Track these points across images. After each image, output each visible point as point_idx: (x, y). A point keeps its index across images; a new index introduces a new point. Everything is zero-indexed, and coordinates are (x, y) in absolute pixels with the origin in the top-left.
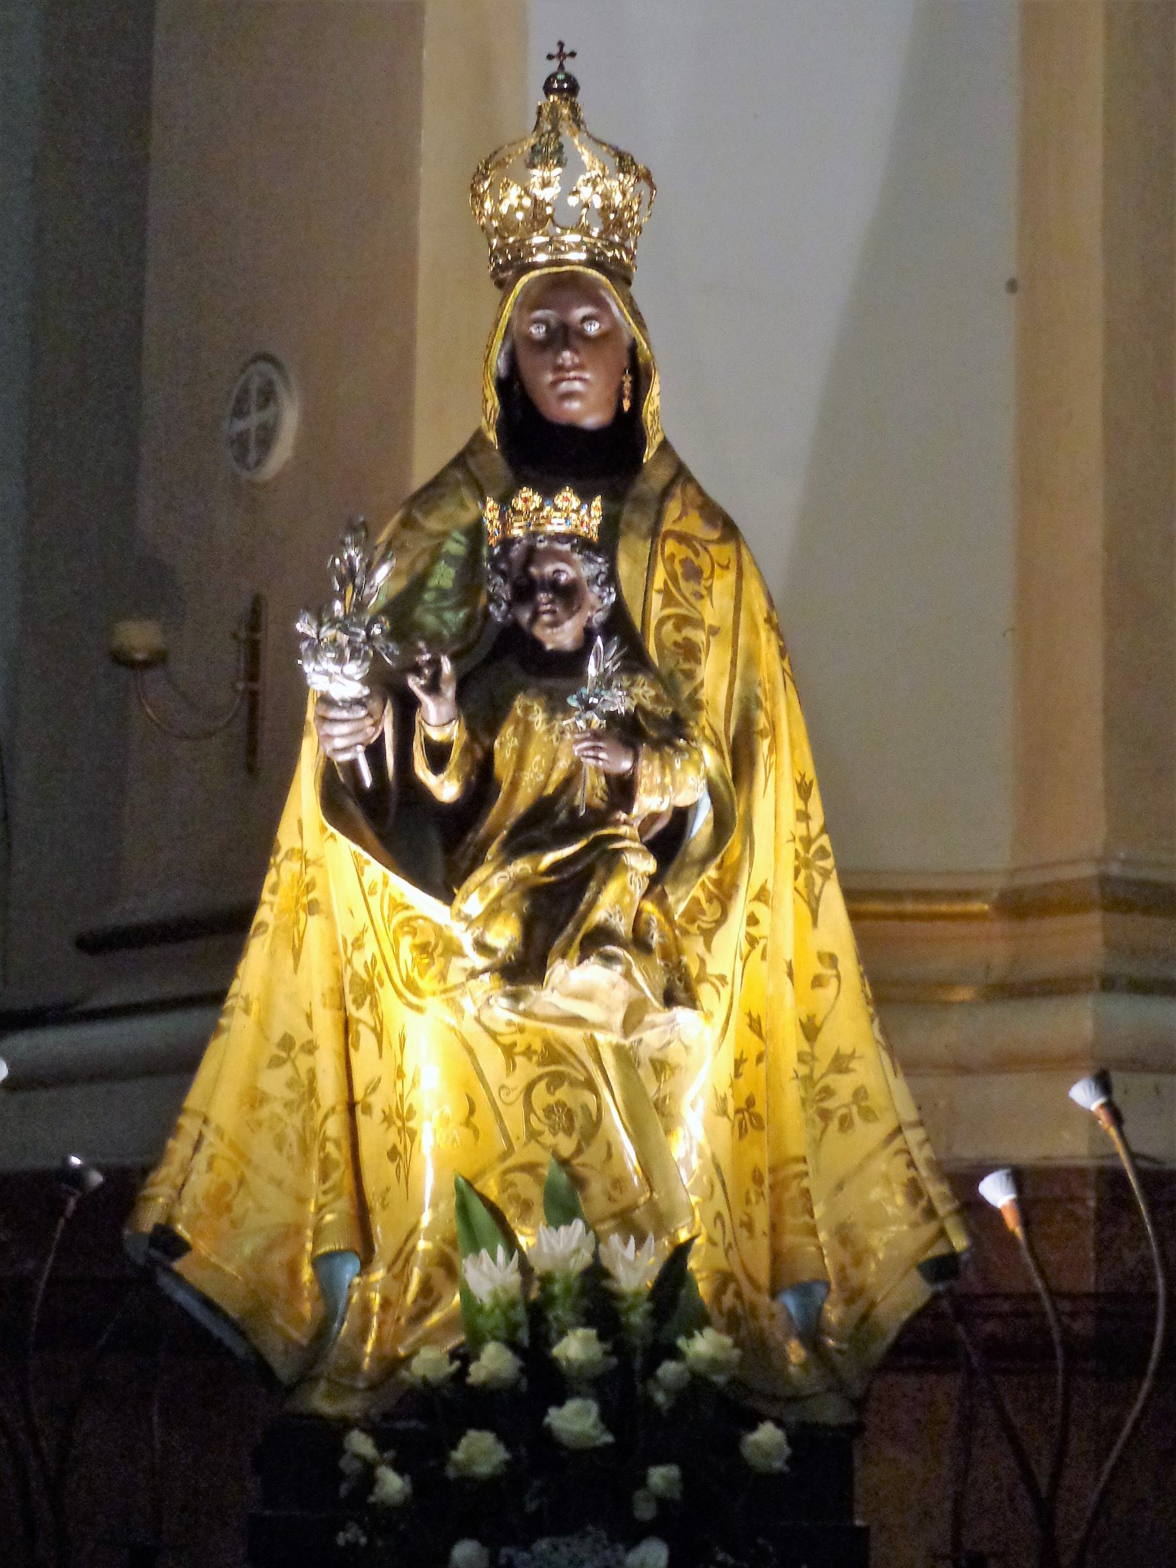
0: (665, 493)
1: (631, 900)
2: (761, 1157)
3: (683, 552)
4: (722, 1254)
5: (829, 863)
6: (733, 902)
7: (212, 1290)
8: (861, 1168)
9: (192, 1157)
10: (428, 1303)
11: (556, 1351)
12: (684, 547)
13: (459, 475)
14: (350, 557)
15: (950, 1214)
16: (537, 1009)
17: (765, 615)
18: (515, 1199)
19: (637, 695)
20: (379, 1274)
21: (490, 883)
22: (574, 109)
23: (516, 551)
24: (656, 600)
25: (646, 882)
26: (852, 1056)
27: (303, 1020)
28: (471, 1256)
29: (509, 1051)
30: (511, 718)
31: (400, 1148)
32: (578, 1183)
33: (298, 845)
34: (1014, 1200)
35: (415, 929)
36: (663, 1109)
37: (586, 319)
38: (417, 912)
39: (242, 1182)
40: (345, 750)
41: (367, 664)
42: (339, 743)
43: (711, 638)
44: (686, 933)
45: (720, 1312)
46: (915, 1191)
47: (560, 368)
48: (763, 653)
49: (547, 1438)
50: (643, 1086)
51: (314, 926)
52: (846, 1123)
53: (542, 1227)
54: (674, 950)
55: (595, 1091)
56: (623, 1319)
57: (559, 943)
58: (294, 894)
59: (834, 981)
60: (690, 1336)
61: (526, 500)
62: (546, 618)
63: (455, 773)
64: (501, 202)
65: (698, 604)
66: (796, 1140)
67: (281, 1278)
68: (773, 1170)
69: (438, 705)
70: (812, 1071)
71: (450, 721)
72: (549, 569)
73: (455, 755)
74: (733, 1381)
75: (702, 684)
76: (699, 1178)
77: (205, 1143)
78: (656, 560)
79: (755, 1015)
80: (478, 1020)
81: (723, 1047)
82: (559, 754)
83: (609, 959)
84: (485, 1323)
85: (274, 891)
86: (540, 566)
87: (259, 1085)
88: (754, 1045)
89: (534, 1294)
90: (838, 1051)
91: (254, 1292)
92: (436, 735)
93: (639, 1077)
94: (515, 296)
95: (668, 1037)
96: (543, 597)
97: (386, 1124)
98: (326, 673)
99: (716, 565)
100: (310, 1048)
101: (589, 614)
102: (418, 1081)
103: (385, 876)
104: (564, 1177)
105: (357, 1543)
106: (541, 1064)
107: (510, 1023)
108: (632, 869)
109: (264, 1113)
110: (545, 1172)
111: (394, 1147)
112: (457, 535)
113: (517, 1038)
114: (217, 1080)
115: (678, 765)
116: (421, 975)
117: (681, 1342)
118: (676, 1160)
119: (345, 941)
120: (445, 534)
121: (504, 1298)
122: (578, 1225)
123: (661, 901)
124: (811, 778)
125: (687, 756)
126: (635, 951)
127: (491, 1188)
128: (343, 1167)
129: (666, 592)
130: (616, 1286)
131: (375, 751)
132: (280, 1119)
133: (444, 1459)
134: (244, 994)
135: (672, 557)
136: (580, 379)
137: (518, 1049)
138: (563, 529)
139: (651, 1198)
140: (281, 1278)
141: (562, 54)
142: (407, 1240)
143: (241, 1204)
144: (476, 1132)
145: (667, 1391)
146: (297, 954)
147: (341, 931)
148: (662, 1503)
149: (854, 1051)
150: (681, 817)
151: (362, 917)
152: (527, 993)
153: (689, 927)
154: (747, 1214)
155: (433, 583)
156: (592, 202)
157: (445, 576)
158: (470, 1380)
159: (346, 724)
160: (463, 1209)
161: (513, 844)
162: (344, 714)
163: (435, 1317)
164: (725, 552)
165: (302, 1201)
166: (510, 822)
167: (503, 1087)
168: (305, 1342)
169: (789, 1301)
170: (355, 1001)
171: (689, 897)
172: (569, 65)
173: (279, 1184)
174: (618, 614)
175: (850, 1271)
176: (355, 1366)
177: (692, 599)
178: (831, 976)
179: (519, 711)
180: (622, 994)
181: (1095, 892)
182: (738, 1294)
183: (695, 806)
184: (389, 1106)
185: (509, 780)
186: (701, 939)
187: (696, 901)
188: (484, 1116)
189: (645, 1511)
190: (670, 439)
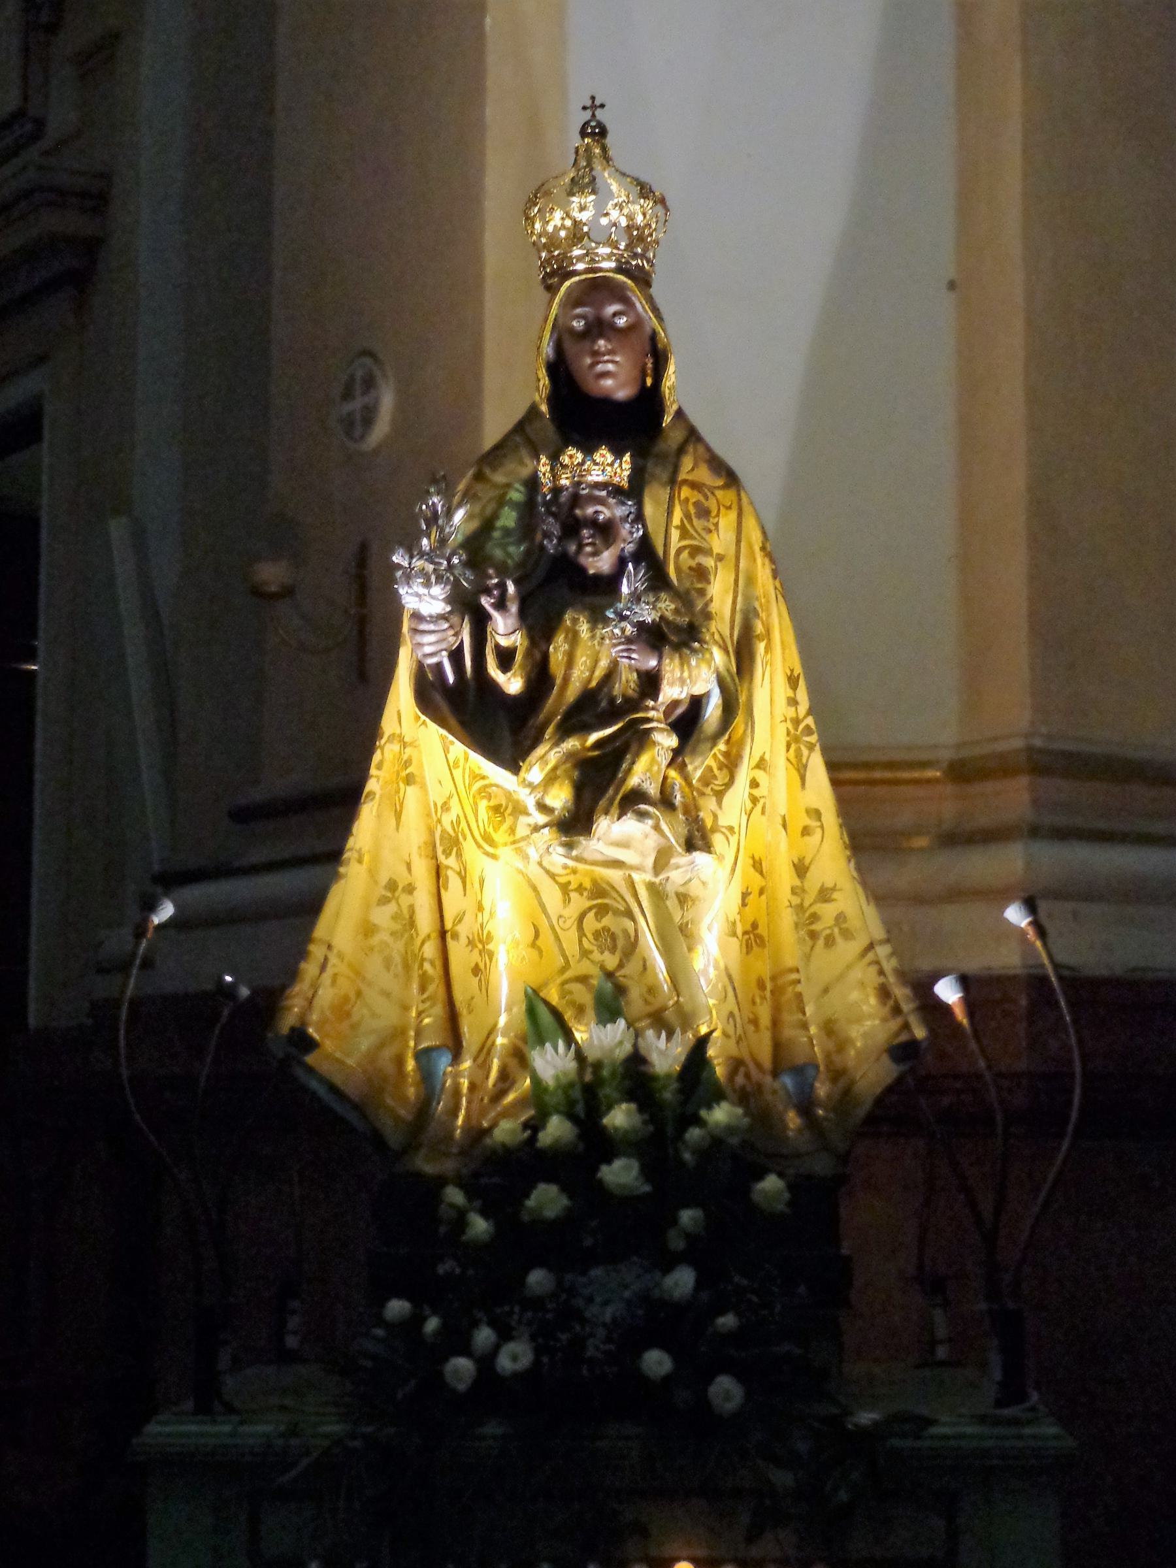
0: (681, 450)
2: (763, 968)
3: (695, 496)
5: (813, 739)
6: (738, 769)
8: (841, 977)
11: (605, 1121)
12: (696, 493)
13: (518, 439)
14: (433, 503)
16: (586, 855)
17: (761, 545)
18: (572, 1003)
19: (660, 608)
20: (467, 1064)
22: (604, 149)
23: (564, 497)
26: (834, 889)
27: (404, 868)
29: (565, 888)
31: (482, 966)
32: (621, 990)
33: (398, 731)
36: (686, 931)
37: (615, 314)
39: (359, 994)
40: (432, 655)
41: (448, 587)
42: (428, 650)
44: (703, 794)
46: (884, 993)
48: (759, 574)
52: (830, 942)
53: (593, 1025)
55: (633, 919)
57: (603, 803)
58: (395, 770)
59: (819, 831)
60: (709, 1107)
61: (571, 457)
62: (588, 549)
63: (519, 672)
66: (791, 958)
67: (390, 1068)
68: (773, 978)
69: (505, 618)
70: (802, 900)
71: (513, 632)
72: (590, 510)
73: (519, 657)
75: (711, 600)
77: (329, 965)
79: (757, 858)
80: (540, 864)
83: (642, 815)
84: (551, 1100)
85: (379, 767)
86: (582, 508)
88: (757, 881)
89: (588, 1077)
92: (504, 642)
96: (585, 532)
97: (470, 948)
98: (417, 595)
100: (410, 889)
101: (622, 546)
103: (465, 753)
104: (609, 985)
106: (590, 898)
107: (565, 867)
109: (375, 940)
110: (595, 982)
111: (477, 965)
112: (517, 486)
114: (337, 915)
115: (693, 663)
116: (495, 830)
117: (703, 1113)
119: (435, 805)
120: (508, 486)
121: (564, 1081)
122: (621, 1023)
123: (682, 768)
125: (700, 655)
127: (554, 997)
128: (437, 981)
131: (456, 656)
134: (357, 847)
135: (687, 500)
136: (612, 362)
138: (600, 479)
139: (677, 1002)
141: (594, 106)
142: (488, 1037)
143: (359, 1012)
146: (398, 815)
147: (432, 798)
148: (687, 1236)
150: (697, 703)
152: (579, 842)
155: (500, 523)
159: (433, 635)
160: (531, 1012)
162: (432, 627)
163: (511, 1097)
165: (406, 1008)
167: (560, 916)
169: (788, 1081)
170: (444, 852)
172: (599, 113)
173: (387, 994)
176: (450, 1136)
177: (703, 534)
180: (652, 842)
182: (747, 1076)
183: (707, 695)
185: (561, 676)
186: (714, 799)
188: (547, 939)
189: (677, 1243)
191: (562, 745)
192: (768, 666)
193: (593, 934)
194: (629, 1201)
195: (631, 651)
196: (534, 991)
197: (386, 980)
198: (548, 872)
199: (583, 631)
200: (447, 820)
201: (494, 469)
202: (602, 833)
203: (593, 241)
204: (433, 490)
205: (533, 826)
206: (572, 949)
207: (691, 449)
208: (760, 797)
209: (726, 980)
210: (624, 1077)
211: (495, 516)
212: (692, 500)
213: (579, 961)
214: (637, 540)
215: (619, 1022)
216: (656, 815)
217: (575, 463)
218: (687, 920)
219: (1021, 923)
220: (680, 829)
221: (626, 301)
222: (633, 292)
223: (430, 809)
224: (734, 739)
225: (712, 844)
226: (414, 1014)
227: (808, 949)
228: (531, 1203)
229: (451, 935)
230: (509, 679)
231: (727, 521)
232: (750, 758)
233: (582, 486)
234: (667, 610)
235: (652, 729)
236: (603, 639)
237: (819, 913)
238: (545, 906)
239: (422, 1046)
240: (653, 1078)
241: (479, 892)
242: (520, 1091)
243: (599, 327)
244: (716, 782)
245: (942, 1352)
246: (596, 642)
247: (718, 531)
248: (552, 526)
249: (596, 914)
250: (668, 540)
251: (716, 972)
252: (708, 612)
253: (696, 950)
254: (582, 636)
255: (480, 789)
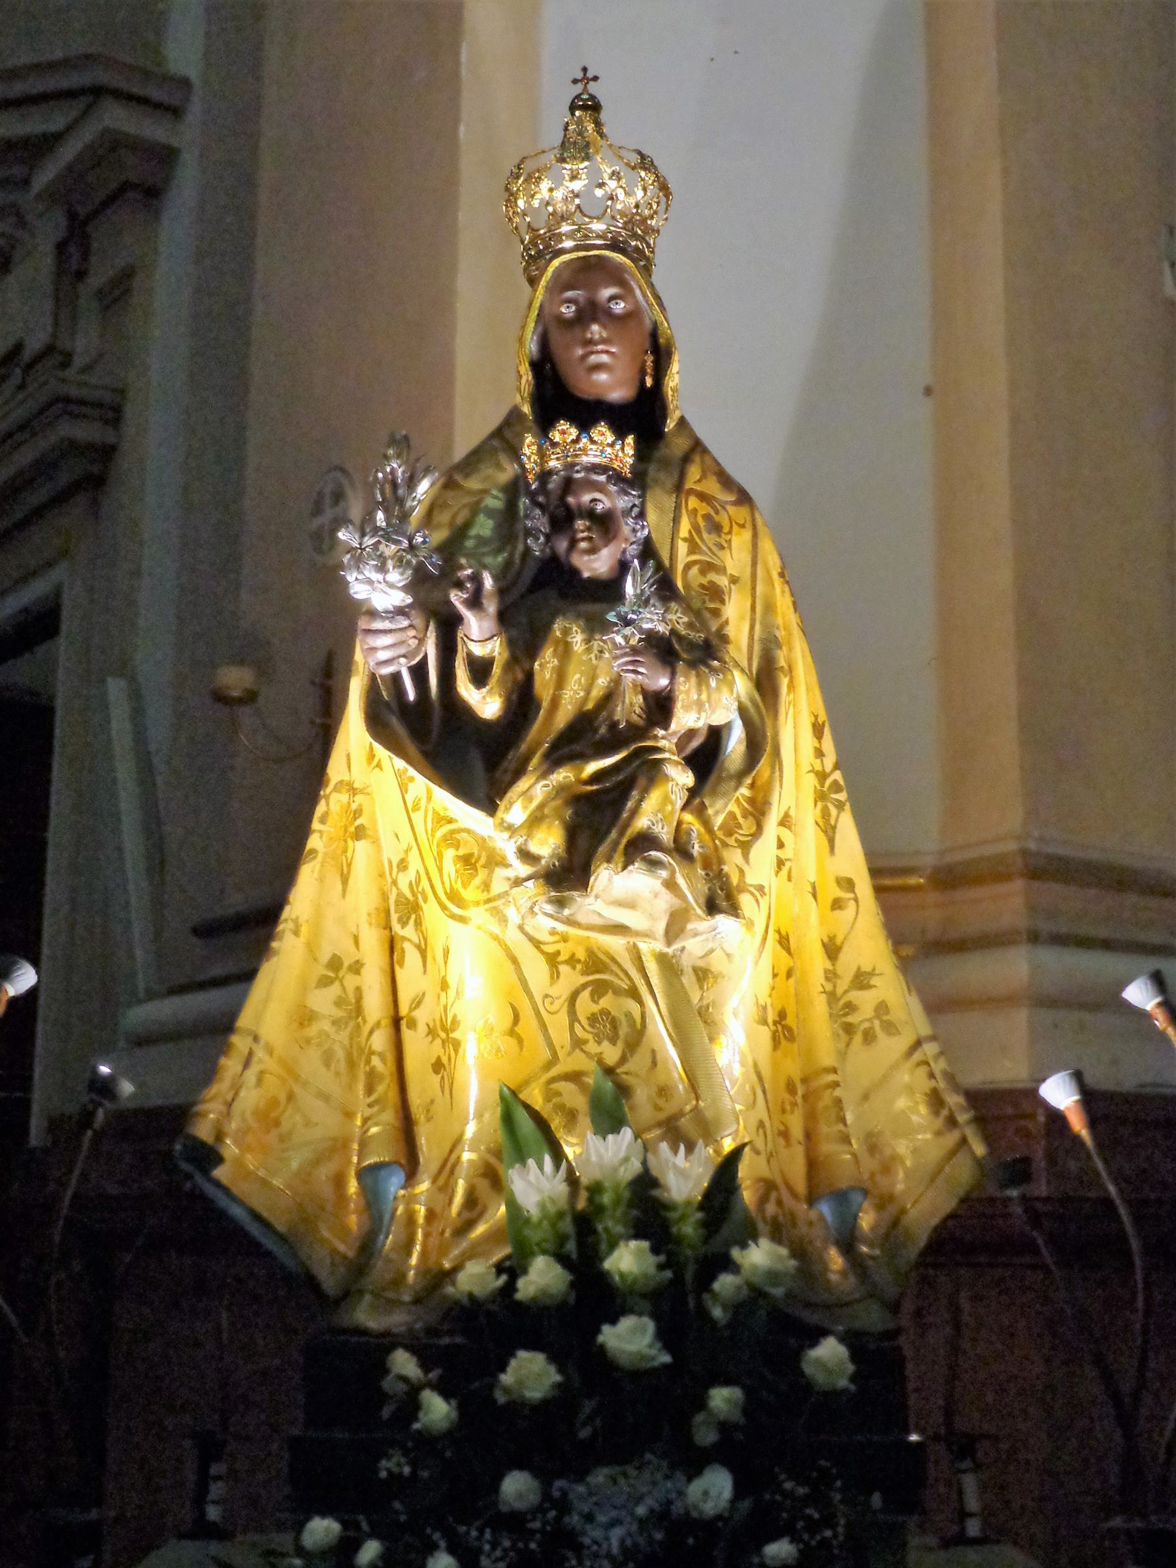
0: (686, 459)
1: (672, 809)
2: (793, 1068)
3: (704, 509)
4: (764, 1162)
5: (842, 796)
6: (767, 818)
7: (258, 1203)
8: (885, 1079)
9: (242, 1073)
10: (474, 1214)
11: (608, 1264)
12: (704, 504)
13: (495, 443)
14: (393, 469)
15: (969, 1122)
16: (581, 918)
17: (780, 570)
18: (560, 1108)
19: (671, 620)
20: (423, 1186)
21: (532, 791)
22: (598, 124)
23: (554, 484)
24: (682, 548)
25: (685, 795)
26: (872, 974)
27: (351, 942)
28: (517, 1166)
29: (552, 960)
30: (550, 638)
31: (445, 1060)
32: (623, 1091)
33: (347, 778)
34: (1077, 1102)
35: (458, 841)
36: (707, 1017)
37: (612, 298)
38: (461, 825)
39: (291, 1097)
40: (387, 662)
41: (409, 572)
42: (383, 655)
43: (732, 585)
44: (725, 845)
45: (764, 1218)
46: (936, 1101)
47: (590, 342)
48: (779, 604)
49: (601, 1358)
50: (686, 993)
51: (361, 850)
52: (869, 1037)
53: (590, 1135)
54: (715, 861)
55: (641, 1002)
56: (674, 1230)
57: (603, 849)
58: (342, 824)
59: (852, 903)
60: (744, 1246)
61: (563, 432)
62: (583, 545)
63: (496, 690)
64: (533, 196)
65: (720, 553)
66: (826, 1056)
67: (327, 1191)
68: (805, 1081)
69: (480, 620)
70: (835, 986)
71: (491, 638)
72: (586, 498)
73: (497, 670)
74: (789, 1295)
75: (727, 622)
76: (743, 1086)
77: (255, 1059)
78: (680, 512)
79: (784, 933)
80: (521, 928)
81: (764, 955)
82: (598, 671)
83: (654, 864)
84: (534, 1236)
85: (323, 821)
86: (576, 495)
87: (309, 1005)
88: (785, 961)
89: (581, 1204)
90: (859, 968)
91: (300, 1205)
92: (479, 651)
93: (682, 985)
94: (548, 279)
95: (710, 945)
96: (580, 524)
97: (430, 1038)
98: (370, 582)
99: (734, 523)
100: (357, 968)
101: (624, 546)
102: (462, 991)
103: (429, 792)
104: (609, 1085)
105: (401, 1474)
106: (585, 973)
107: (553, 932)
108: (673, 780)
109: (313, 1030)
110: (590, 1081)
111: (439, 1059)
112: (495, 492)
113: (560, 946)
114: (266, 1001)
115: (713, 683)
116: (465, 886)
117: (735, 1253)
118: (720, 1066)
119: (390, 863)
120: (485, 492)
121: (552, 1209)
122: (627, 1133)
123: (701, 812)
124: (823, 719)
125: (721, 676)
126: (678, 857)
127: (535, 1097)
128: (387, 1081)
129: (690, 540)
130: (666, 1194)
131: (419, 672)
132: (328, 1036)
133: (494, 1383)
134: (294, 916)
135: (695, 511)
136: (607, 352)
137: (561, 958)
138: (597, 460)
139: (696, 1107)
140: (327, 1191)
141: (586, 78)
142: (451, 1151)
143: (290, 1119)
144: (520, 1041)
145: (725, 1307)
146: (345, 880)
147: (386, 855)
148: (724, 1427)
149: (874, 969)
150: (716, 735)
151: (407, 836)
152: (572, 899)
153: (728, 840)
154: (782, 1123)
155: (473, 532)
156: (616, 195)
157: (484, 527)
158: (519, 1296)
159: (389, 636)
160: (508, 1119)
161: (555, 756)
162: (387, 625)
163: (480, 1229)
164: (740, 513)
165: (349, 1115)
166: (552, 736)
167: (547, 996)
168: (351, 1254)
169: (825, 1209)
170: (400, 920)
171: (726, 812)
172: (593, 87)
173: (325, 1097)
174: (648, 551)
175: (878, 1178)
176: (399, 1280)
177: (714, 549)
178: (849, 899)
179: (558, 634)
180: (664, 902)
181: (1019, 862)
182: (779, 1203)
183: (728, 726)
184: (434, 1019)
185: (549, 699)
186: (739, 851)
187: (732, 815)
188: (528, 1025)
189: (706, 1436)
190: (687, 417)
191: (551, 777)
192: (792, 706)
193: (588, 1019)
194: (641, 1376)
195: (638, 664)
196: (514, 1093)
197: (325, 1079)
198: (531, 939)
199: (577, 642)
200: (404, 880)
201: (467, 476)
202: (601, 888)
203: (585, 216)
204: (392, 452)
205: (513, 880)
206: (560, 1034)
207: (697, 459)
208: (786, 860)
209: (755, 1078)
210: (631, 1205)
211: (467, 525)
212: (701, 512)
213: (569, 1054)
214: (642, 541)
215: (625, 1132)
216: (670, 864)
217: (568, 441)
218: (708, 1001)
219: (1146, 1004)
220: (699, 886)
221: (622, 283)
222: (633, 276)
223: (384, 868)
224: (759, 783)
225: (739, 905)
226: (359, 1123)
227: (842, 1045)
228: (507, 1378)
229: (407, 1023)
230: (484, 698)
231: (740, 540)
232: (779, 806)
233: (576, 468)
234: (678, 623)
235: (664, 760)
236: (601, 652)
237: (854, 1003)
238: (527, 983)
239: (367, 1163)
240: (668, 1206)
241: (442, 962)
242: (492, 1221)
243: (591, 312)
244: (741, 832)
245: (973, 1528)
246: (593, 656)
247: (731, 550)
248: (540, 522)
249: (592, 995)
250: (674, 562)
251: (744, 1069)
252: (724, 634)
253: (718, 1041)
254: (576, 649)
255: (445, 836)
